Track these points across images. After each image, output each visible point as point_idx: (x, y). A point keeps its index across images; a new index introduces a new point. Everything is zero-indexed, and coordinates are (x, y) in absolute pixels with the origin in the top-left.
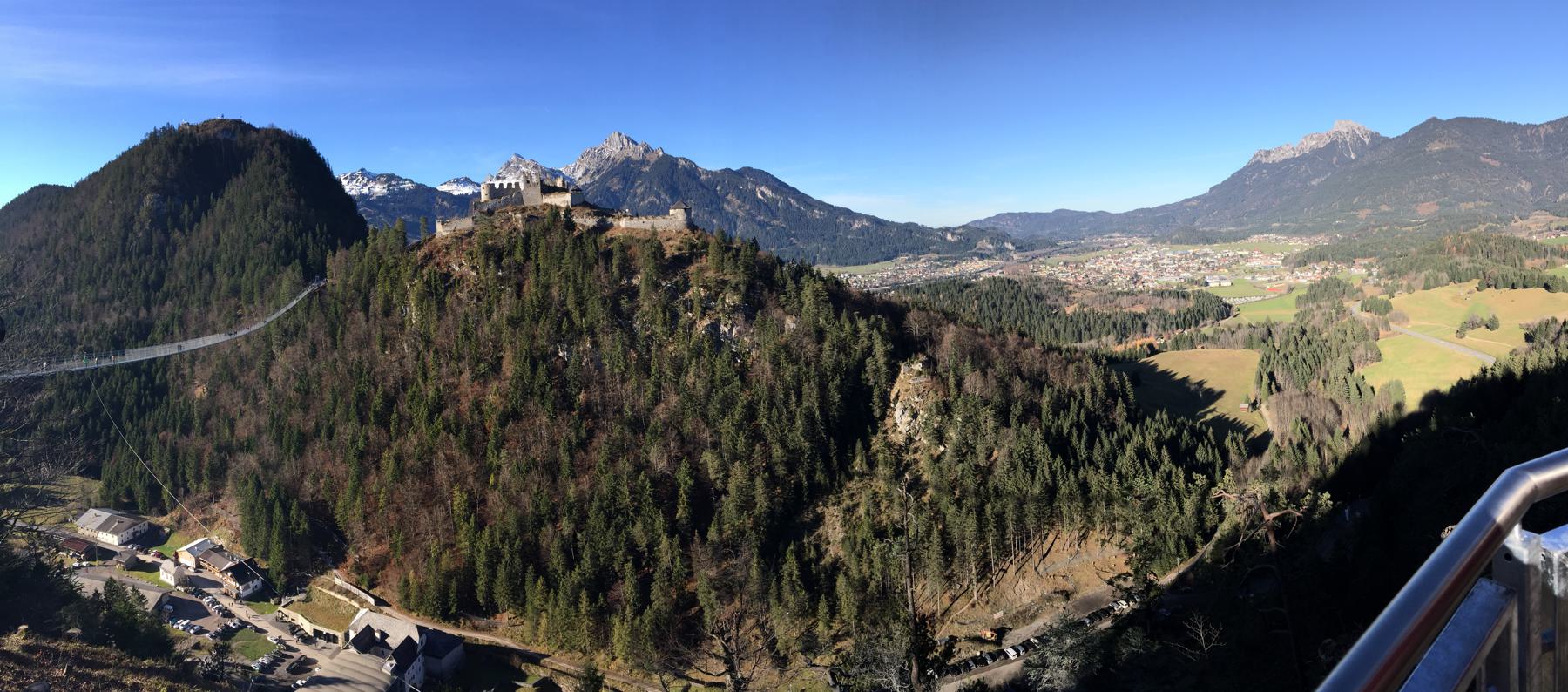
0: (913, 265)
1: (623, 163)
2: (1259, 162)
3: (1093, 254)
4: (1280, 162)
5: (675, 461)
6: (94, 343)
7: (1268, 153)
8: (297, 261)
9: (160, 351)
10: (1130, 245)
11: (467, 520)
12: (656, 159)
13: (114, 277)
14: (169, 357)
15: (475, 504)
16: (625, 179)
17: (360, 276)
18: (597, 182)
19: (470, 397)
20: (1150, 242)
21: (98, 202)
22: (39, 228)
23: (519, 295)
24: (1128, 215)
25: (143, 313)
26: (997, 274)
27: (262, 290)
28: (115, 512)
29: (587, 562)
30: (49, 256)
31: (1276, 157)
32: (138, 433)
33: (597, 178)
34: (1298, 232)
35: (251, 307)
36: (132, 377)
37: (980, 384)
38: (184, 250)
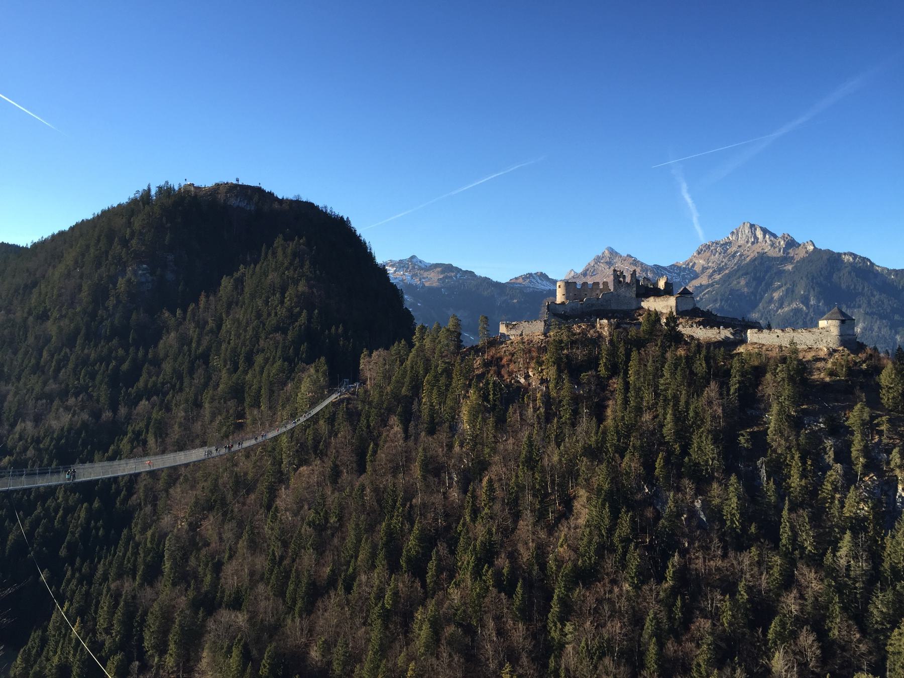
6: (30, 453)
8: (323, 359)
9: (124, 468)
13: (71, 366)
14: (137, 475)
16: (758, 280)
17: (400, 383)
18: (717, 283)
21: (61, 268)
23: (601, 419)
25: (107, 415)
27: (272, 392)
32: (80, 582)
33: (717, 277)
38: (173, 334)
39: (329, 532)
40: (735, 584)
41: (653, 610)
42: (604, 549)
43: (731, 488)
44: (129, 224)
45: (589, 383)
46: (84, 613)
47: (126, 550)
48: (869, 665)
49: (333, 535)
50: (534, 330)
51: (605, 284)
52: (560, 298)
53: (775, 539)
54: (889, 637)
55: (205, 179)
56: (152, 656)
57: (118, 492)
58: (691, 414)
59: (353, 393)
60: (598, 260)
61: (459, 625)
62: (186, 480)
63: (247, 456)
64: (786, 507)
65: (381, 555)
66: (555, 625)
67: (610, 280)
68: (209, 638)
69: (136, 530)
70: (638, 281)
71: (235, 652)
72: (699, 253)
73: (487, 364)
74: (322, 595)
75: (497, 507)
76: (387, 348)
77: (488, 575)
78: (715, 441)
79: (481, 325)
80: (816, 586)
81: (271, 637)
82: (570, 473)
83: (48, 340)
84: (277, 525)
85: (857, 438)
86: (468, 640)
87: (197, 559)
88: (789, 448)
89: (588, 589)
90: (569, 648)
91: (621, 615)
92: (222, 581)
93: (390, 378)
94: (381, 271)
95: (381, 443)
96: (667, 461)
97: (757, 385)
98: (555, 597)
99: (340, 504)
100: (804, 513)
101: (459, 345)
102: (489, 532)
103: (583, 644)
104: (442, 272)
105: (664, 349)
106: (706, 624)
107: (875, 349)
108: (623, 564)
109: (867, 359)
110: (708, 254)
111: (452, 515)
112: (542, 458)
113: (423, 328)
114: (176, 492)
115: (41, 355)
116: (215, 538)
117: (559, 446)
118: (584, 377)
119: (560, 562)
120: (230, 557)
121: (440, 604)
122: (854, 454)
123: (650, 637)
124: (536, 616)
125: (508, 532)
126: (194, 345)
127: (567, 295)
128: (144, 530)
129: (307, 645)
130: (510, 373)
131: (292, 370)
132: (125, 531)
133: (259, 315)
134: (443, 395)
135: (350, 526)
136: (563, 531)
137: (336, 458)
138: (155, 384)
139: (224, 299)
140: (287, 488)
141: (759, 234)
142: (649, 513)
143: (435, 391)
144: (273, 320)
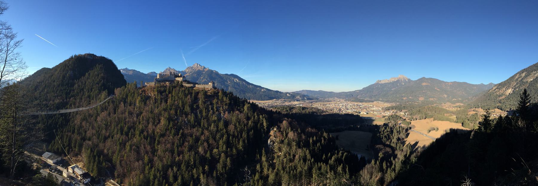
0: (277, 102)
1: (198, 71)
2: (378, 83)
3: (329, 103)
4: (383, 84)
5: (206, 152)
6: (52, 107)
7: (380, 81)
8: (107, 90)
9: (68, 111)
10: (339, 101)
11: (148, 165)
12: (207, 70)
13: (59, 91)
14: (71, 112)
15: (151, 161)
17: (123, 95)
19: (151, 129)
20: (345, 101)
21: (57, 72)
22: (42, 78)
23: (167, 103)
24: (339, 93)
25: (65, 100)
26: (301, 105)
27: (96, 97)
28: (53, 154)
29: (179, 180)
30: (44, 85)
31: (383, 82)
32: (61, 132)
33: (190, 74)
34: (387, 101)
35: (93, 101)
36: (61, 117)
37: (293, 135)
38: (77, 85)
39: (108, 126)
40: (193, 135)
41: (176, 141)
42: (167, 130)
43: (192, 116)
44: (69, 63)
45: (164, 95)
46: (62, 138)
47: (69, 127)
48: (216, 147)
49: (109, 127)
50: (153, 84)
51: (168, 74)
52: (158, 77)
53: (200, 125)
54: (219, 142)
55: (83, 53)
56: (73, 148)
57: (67, 116)
58: (185, 101)
59: (113, 97)
60: (167, 69)
61: (136, 146)
62: (79, 114)
63: (91, 110)
64: (202, 119)
65: (119, 131)
66: (156, 145)
67: (169, 74)
68: (84, 146)
69: (71, 123)
70: (175, 74)
71: (89, 149)
72: (187, 69)
73: (142, 91)
74: (107, 139)
75: (144, 121)
76: (121, 88)
77: (142, 136)
78: (189, 107)
79: (141, 83)
80: (207, 134)
81: (96, 147)
82: (160, 114)
83: (55, 86)
84: (97, 124)
85: (215, 105)
86: (138, 149)
87: (82, 130)
88: (203, 108)
89: (163, 138)
90: (159, 150)
91: (170, 143)
92: (87, 135)
93: (121, 94)
94: (119, 71)
95: (119, 108)
96: (180, 111)
97: (198, 96)
98: (156, 140)
99: (110, 120)
100: (205, 120)
101: (136, 87)
102: (143, 127)
103: (162, 149)
104: (133, 71)
105: (180, 88)
106: (187, 143)
107: (218, 89)
108: (171, 132)
109: (217, 90)
110: (189, 69)
111: (134, 123)
112: (154, 111)
113: (128, 83)
114: (77, 116)
115: (54, 88)
116: (85, 126)
117: (158, 108)
118: (163, 94)
119: (157, 133)
120: (88, 130)
121: (132, 142)
122: (214, 108)
123: (176, 147)
124: (152, 144)
125: (146, 127)
126: (81, 87)
127: (160, 76)
128: (72, 123)
129: (104, 149)
130: (147, 93)
131: (100, 92)
132: (69, 123)
133: (93, 81)
134: (133, 97)
135: (113, 125)
136: (158, 126)
137: (110, 111)
138: (73, 94)
139: (86, 77)
140: (99, 117)
141: (199, 65)
142: (176, 122)
143: (131, 97)
144: (96, 82)
